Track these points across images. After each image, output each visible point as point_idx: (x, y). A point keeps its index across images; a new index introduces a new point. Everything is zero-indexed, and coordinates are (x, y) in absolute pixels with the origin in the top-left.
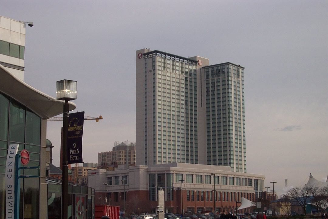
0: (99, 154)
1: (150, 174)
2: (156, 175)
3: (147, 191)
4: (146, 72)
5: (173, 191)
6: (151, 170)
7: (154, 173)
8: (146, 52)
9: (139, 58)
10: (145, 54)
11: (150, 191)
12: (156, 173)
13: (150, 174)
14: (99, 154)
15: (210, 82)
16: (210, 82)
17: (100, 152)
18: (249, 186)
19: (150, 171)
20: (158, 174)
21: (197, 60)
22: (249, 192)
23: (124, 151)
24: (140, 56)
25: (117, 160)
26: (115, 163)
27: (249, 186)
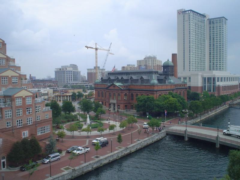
0: (138, 61)
1: (203, 78)
2: (212, 78)
3: (201, 87)
4: (184, 21)
5: (216, 87)
6: (204, 75)
7: (205, 77)
8: (184, 11)
9: (179, 14)
10: (183, 12)
11: (203, 87)
12: (207, 77)
13: (203, 78)
14: (138, 61)
15: (212, 27)
16: (212, 27)
17: (7, 45)
18: (221, 81)
19: (204, 76)
20: (208, 78)
21: (205, 15)
22: (229, 85)
23: (151, 60)
24: (180, 13)
25: (147, 63)
26: (146, 65)
27: (221, 81)
